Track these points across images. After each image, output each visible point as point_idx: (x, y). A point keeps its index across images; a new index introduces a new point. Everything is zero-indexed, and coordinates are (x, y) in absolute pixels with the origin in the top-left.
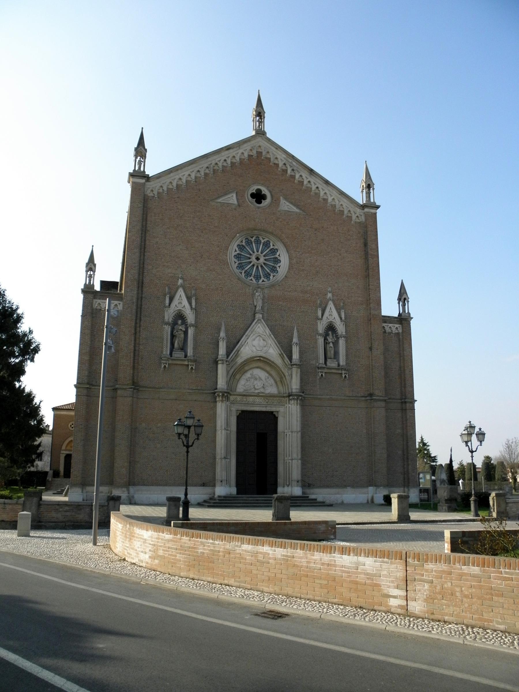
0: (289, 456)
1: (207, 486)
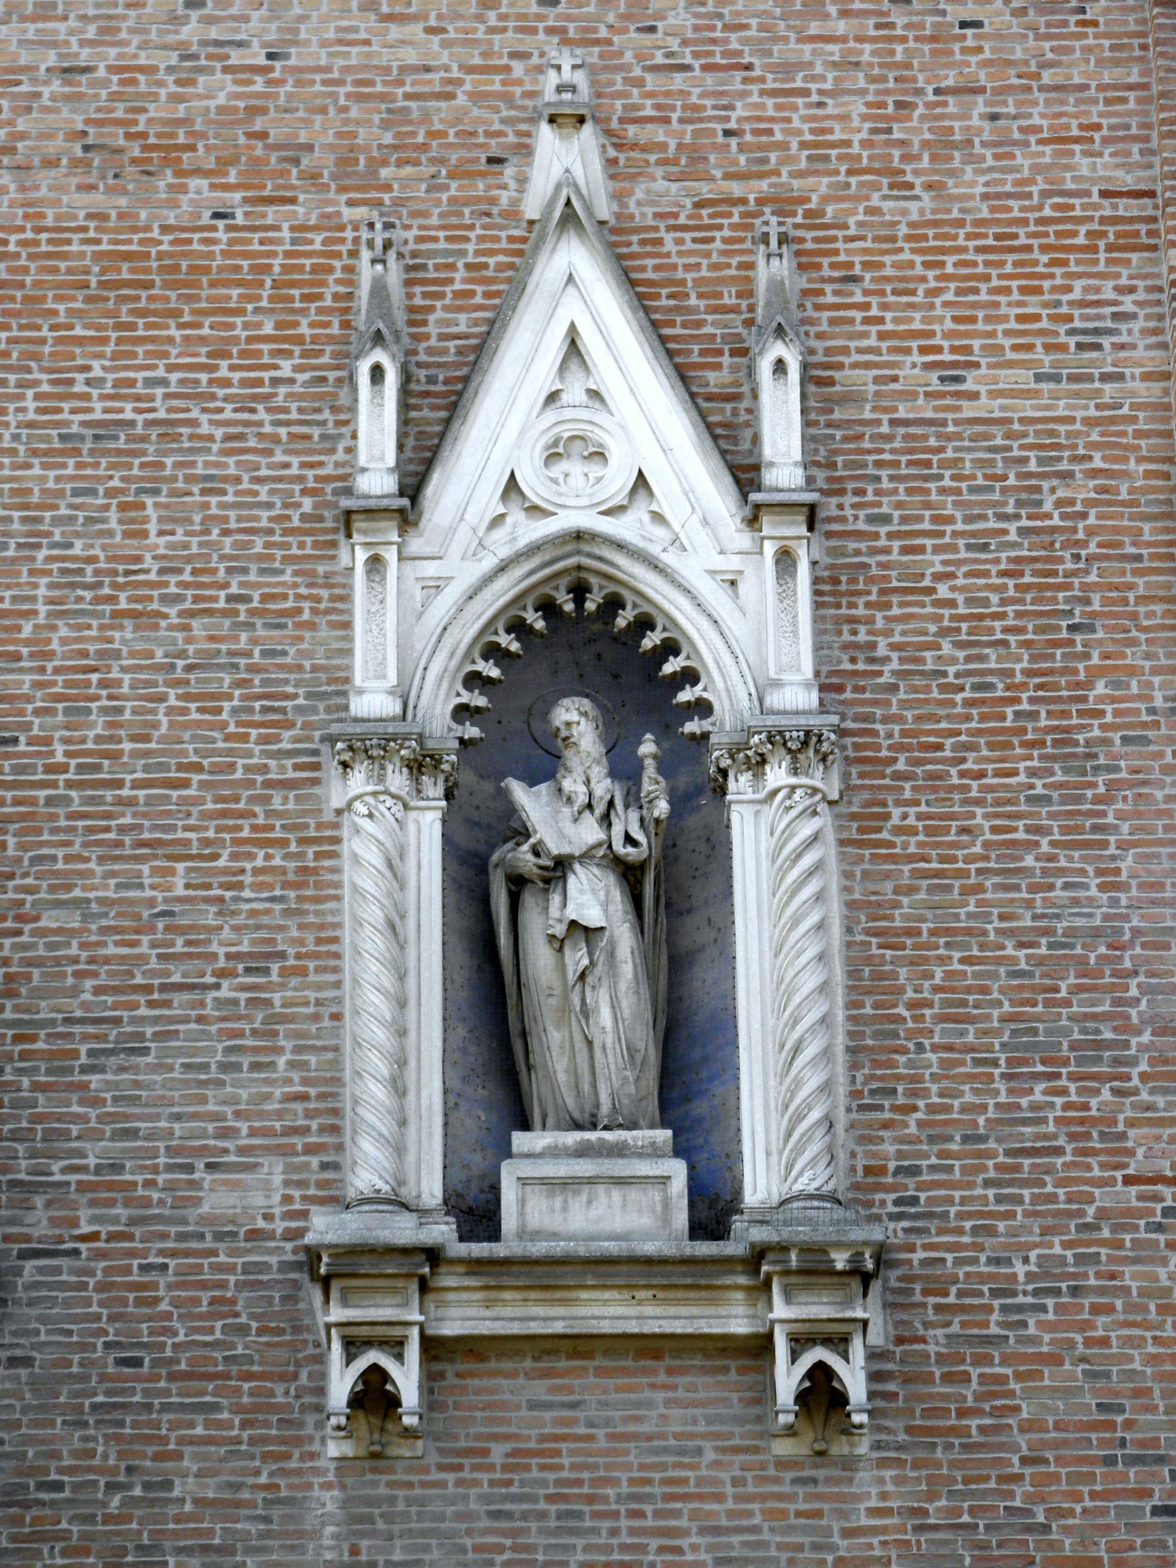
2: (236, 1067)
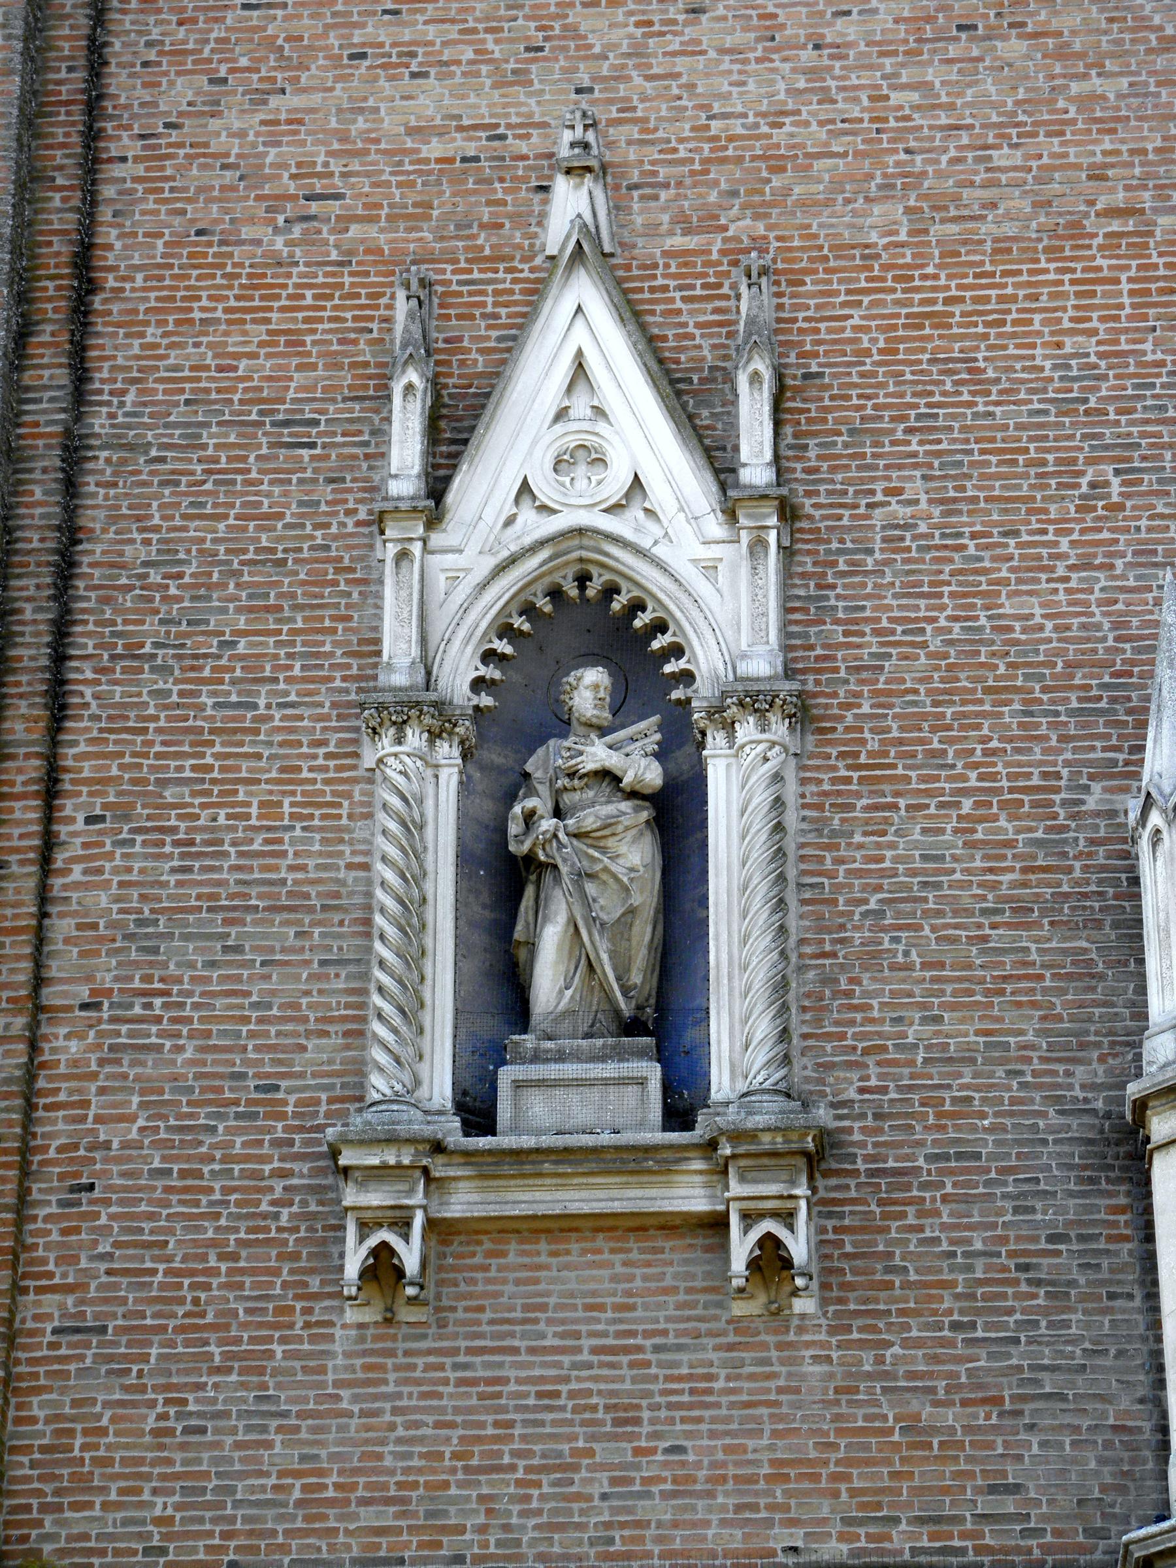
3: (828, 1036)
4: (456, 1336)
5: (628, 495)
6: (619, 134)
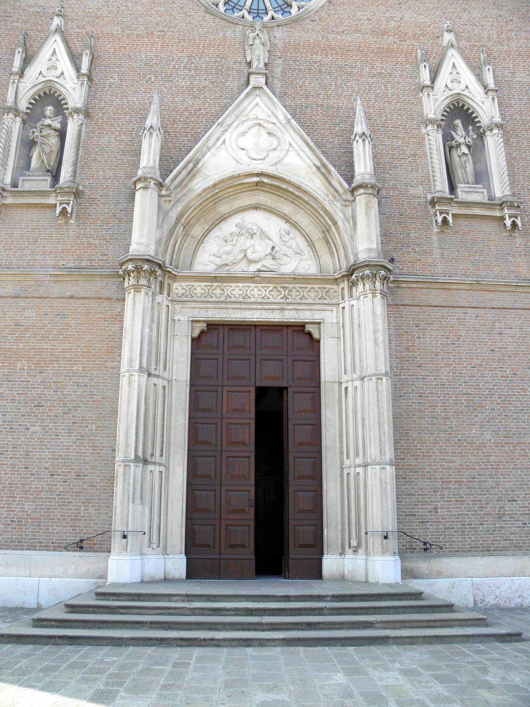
0: (357, 454)
1: (91, 549)
2: (413, 171)
3: (84, 174)
4: (5, 225)
5: (61, 75)
6: (68, 10)
